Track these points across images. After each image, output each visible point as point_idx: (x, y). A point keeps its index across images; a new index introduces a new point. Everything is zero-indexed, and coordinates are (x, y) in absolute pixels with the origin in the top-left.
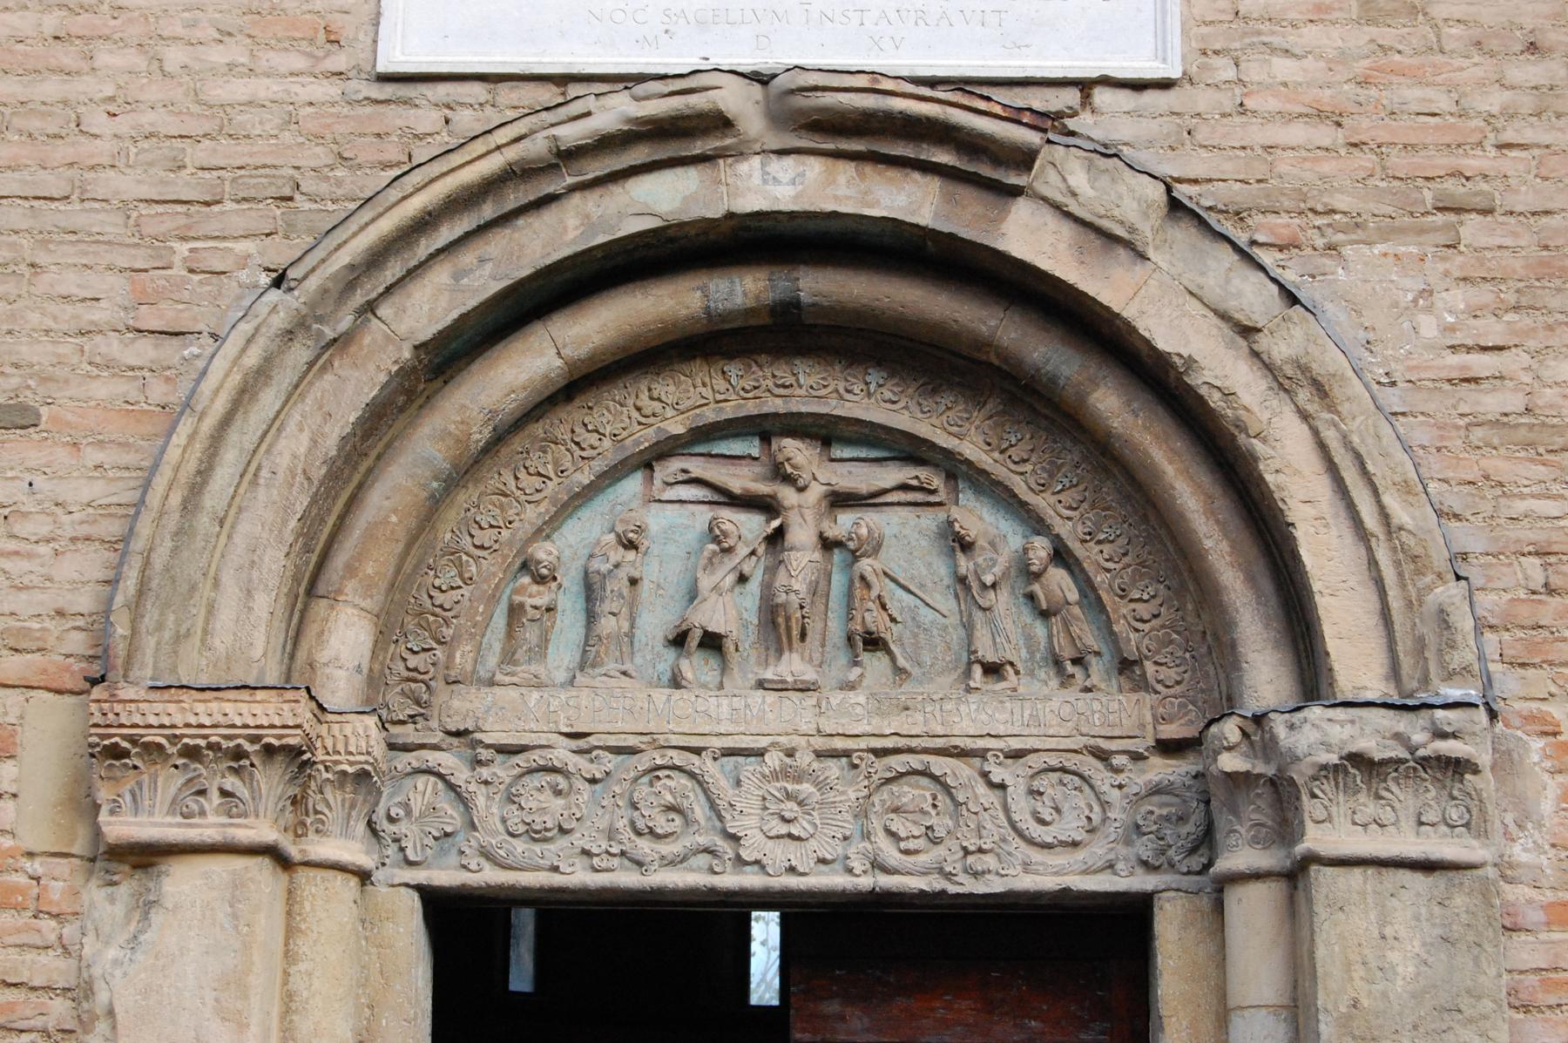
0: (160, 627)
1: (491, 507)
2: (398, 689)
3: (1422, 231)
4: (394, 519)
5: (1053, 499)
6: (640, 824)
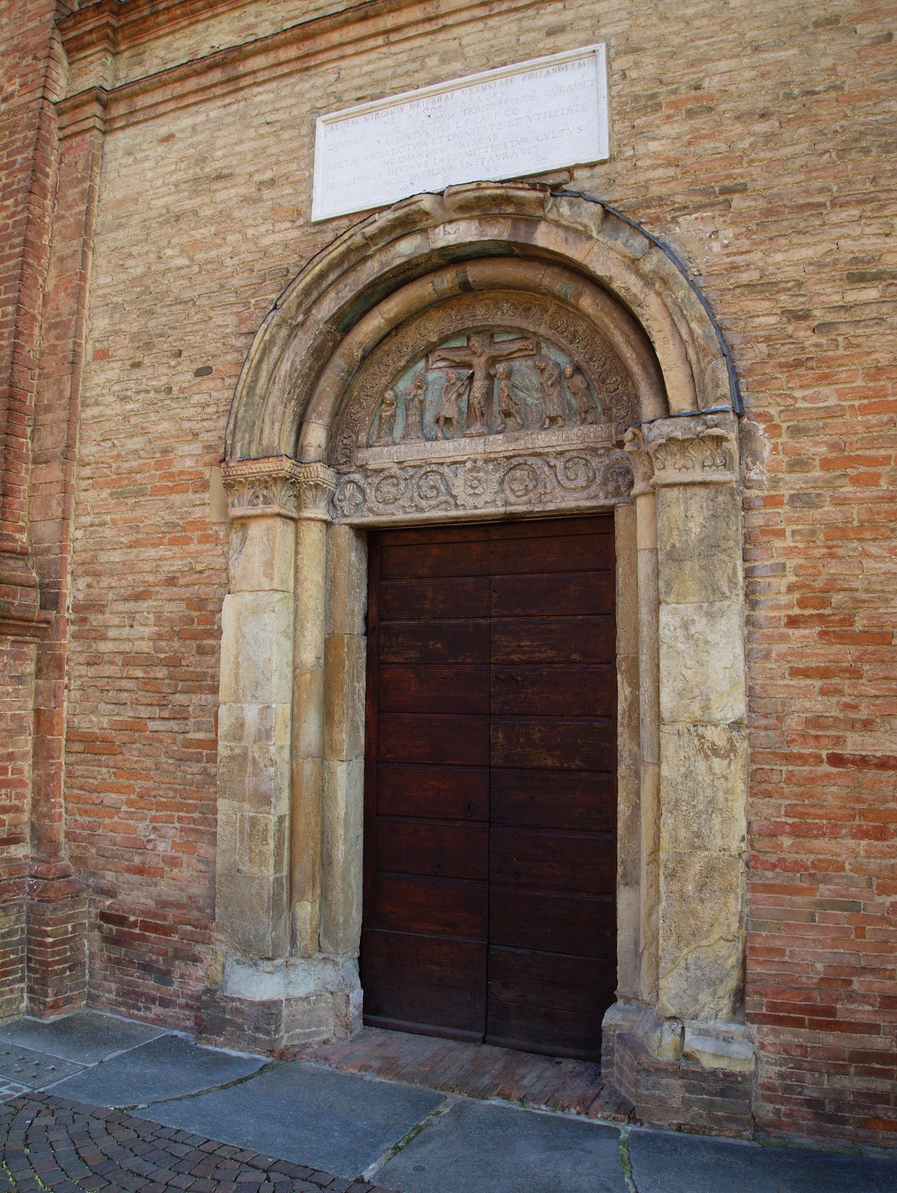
0: (243, 439)
3: (713, 205)
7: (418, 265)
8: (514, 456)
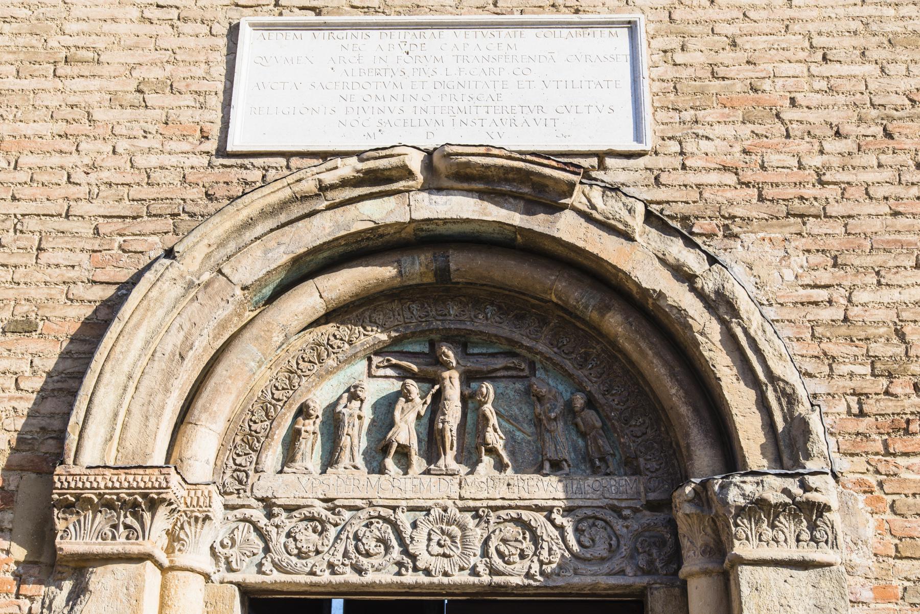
5: (587, 373)
8: (503, 508)
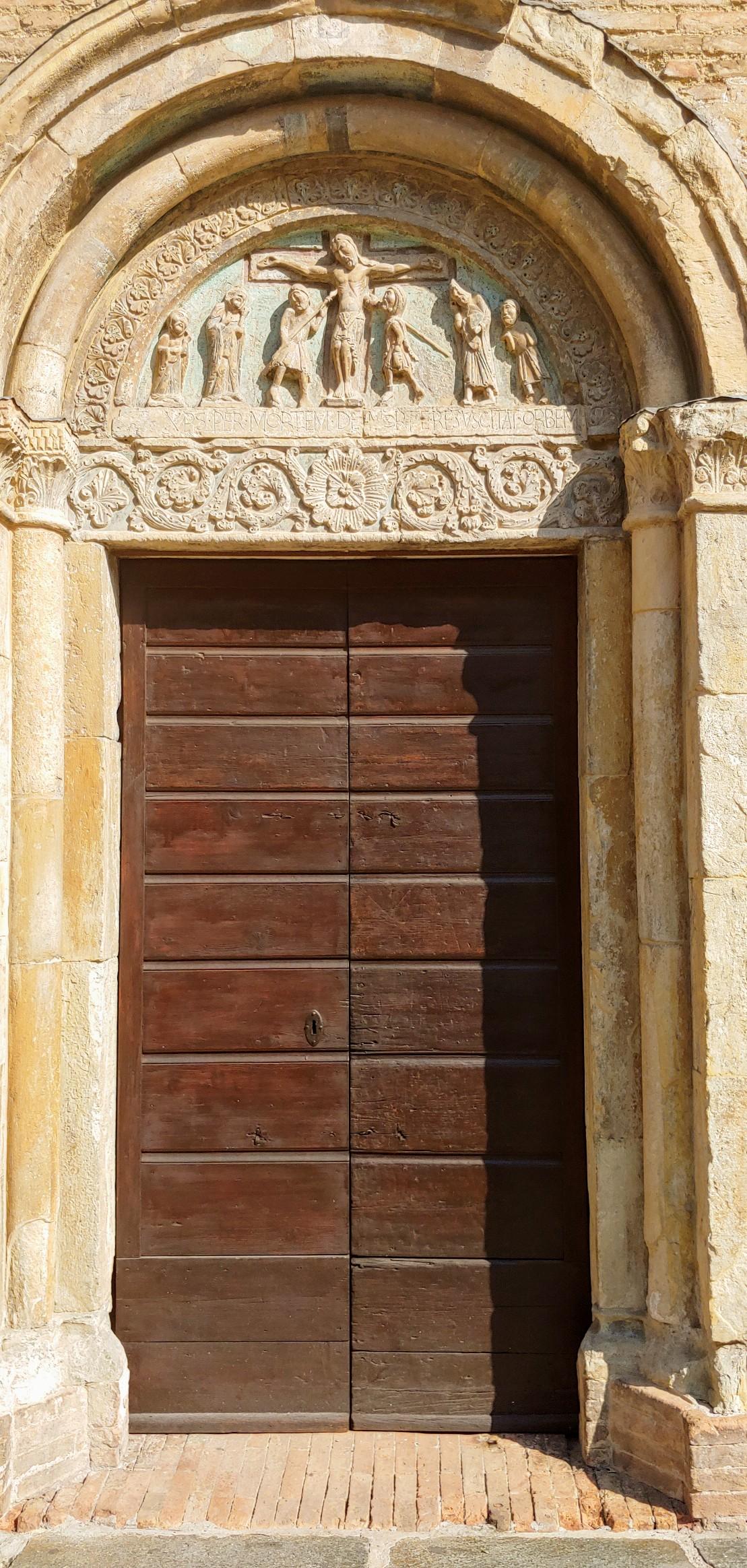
1: (142, 285)
2: (84, 410)
4: (73, 288)
6: (247, 498)
7: (257, 84)
8: (415, 447)
